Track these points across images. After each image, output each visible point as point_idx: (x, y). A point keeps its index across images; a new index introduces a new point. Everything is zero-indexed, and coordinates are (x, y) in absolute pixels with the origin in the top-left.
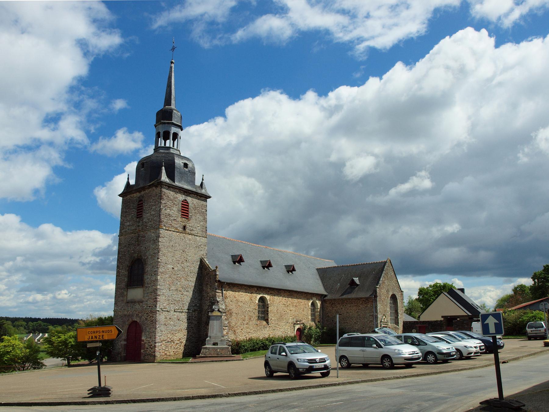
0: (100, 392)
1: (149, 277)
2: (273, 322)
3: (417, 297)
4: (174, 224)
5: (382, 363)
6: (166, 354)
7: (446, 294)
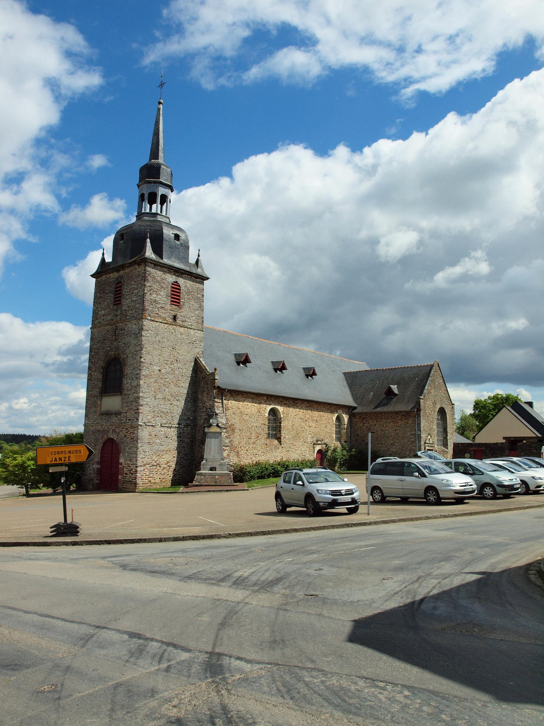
0: (66, 530)
1: (129, 381)
2: (287, 441)
3: (472, 412)
4: (161, 312)
5: (426, 496)
6: (150, 481)
7: (509, 408)
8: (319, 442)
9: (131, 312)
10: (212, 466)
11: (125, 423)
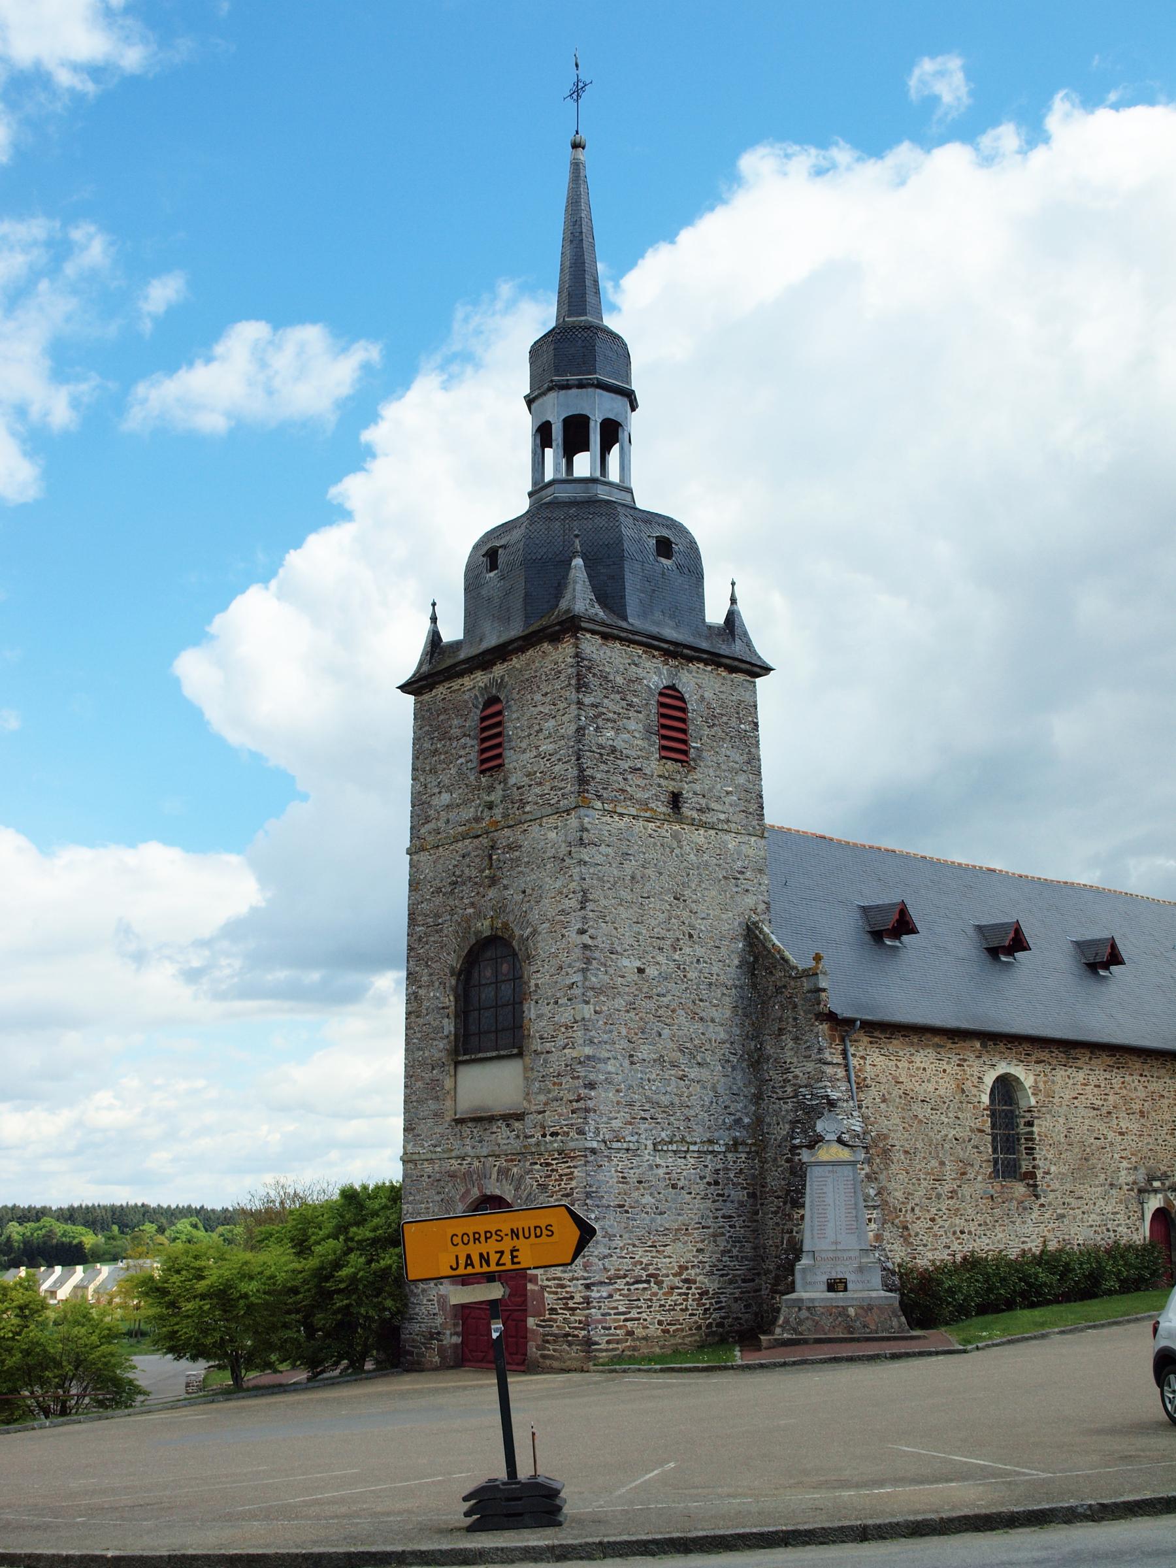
0: (516, 1502)
1: (546, 1010)
2: (1056, 1185)
4: (635, 786)
6: (630, 1333)
8: (1156, 1184)
9: (538, 790)
10: (834, 1276)
11: (538, 1144)
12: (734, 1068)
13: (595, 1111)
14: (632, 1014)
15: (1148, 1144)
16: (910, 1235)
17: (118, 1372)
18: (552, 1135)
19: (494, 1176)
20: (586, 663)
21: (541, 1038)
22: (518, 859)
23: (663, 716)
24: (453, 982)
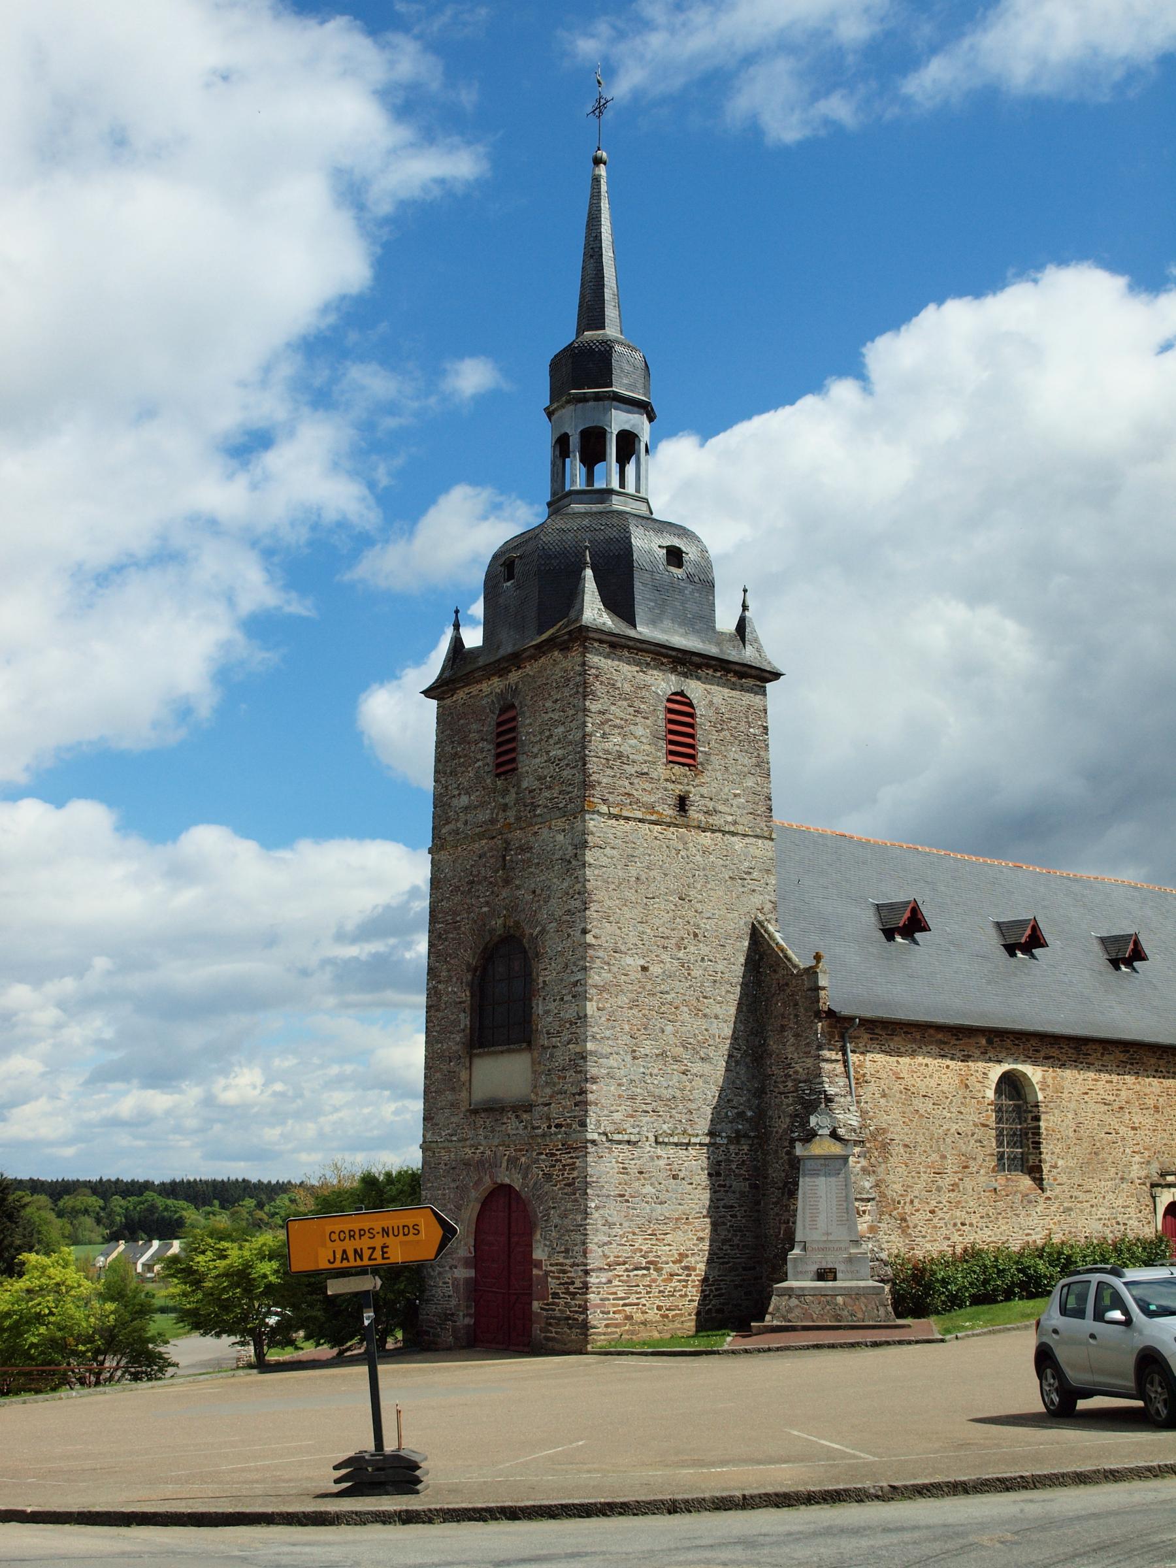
1: (552, 1006)
2: (1063, 1178)
6: (629, 1318)
9: (547, 794)
10: (824, 1265)
11: (544, 1135)
12: (737, 1063)
13: (596, 1104)
14: (635, 1011)
15: (1163, 1138)
16: (908, 1227)
17: (151, 1346)
18: (557, 1126)
19: (504, 1165)
20: (593, 671)
21: (548, 1033)
22: (529, 860)
23: (671, 721)
24: (469, 978)
